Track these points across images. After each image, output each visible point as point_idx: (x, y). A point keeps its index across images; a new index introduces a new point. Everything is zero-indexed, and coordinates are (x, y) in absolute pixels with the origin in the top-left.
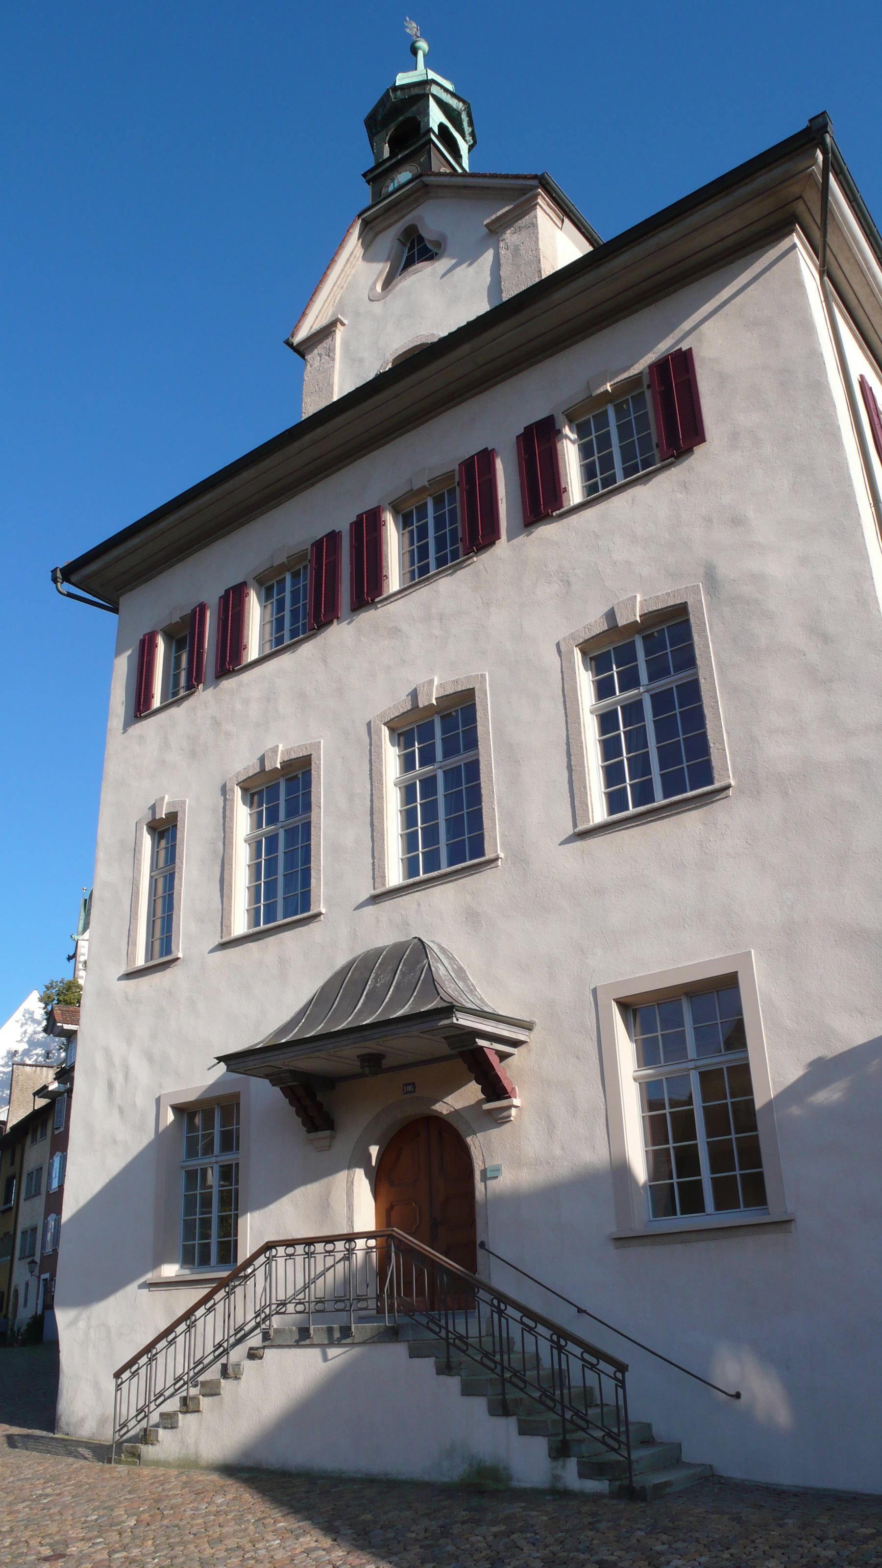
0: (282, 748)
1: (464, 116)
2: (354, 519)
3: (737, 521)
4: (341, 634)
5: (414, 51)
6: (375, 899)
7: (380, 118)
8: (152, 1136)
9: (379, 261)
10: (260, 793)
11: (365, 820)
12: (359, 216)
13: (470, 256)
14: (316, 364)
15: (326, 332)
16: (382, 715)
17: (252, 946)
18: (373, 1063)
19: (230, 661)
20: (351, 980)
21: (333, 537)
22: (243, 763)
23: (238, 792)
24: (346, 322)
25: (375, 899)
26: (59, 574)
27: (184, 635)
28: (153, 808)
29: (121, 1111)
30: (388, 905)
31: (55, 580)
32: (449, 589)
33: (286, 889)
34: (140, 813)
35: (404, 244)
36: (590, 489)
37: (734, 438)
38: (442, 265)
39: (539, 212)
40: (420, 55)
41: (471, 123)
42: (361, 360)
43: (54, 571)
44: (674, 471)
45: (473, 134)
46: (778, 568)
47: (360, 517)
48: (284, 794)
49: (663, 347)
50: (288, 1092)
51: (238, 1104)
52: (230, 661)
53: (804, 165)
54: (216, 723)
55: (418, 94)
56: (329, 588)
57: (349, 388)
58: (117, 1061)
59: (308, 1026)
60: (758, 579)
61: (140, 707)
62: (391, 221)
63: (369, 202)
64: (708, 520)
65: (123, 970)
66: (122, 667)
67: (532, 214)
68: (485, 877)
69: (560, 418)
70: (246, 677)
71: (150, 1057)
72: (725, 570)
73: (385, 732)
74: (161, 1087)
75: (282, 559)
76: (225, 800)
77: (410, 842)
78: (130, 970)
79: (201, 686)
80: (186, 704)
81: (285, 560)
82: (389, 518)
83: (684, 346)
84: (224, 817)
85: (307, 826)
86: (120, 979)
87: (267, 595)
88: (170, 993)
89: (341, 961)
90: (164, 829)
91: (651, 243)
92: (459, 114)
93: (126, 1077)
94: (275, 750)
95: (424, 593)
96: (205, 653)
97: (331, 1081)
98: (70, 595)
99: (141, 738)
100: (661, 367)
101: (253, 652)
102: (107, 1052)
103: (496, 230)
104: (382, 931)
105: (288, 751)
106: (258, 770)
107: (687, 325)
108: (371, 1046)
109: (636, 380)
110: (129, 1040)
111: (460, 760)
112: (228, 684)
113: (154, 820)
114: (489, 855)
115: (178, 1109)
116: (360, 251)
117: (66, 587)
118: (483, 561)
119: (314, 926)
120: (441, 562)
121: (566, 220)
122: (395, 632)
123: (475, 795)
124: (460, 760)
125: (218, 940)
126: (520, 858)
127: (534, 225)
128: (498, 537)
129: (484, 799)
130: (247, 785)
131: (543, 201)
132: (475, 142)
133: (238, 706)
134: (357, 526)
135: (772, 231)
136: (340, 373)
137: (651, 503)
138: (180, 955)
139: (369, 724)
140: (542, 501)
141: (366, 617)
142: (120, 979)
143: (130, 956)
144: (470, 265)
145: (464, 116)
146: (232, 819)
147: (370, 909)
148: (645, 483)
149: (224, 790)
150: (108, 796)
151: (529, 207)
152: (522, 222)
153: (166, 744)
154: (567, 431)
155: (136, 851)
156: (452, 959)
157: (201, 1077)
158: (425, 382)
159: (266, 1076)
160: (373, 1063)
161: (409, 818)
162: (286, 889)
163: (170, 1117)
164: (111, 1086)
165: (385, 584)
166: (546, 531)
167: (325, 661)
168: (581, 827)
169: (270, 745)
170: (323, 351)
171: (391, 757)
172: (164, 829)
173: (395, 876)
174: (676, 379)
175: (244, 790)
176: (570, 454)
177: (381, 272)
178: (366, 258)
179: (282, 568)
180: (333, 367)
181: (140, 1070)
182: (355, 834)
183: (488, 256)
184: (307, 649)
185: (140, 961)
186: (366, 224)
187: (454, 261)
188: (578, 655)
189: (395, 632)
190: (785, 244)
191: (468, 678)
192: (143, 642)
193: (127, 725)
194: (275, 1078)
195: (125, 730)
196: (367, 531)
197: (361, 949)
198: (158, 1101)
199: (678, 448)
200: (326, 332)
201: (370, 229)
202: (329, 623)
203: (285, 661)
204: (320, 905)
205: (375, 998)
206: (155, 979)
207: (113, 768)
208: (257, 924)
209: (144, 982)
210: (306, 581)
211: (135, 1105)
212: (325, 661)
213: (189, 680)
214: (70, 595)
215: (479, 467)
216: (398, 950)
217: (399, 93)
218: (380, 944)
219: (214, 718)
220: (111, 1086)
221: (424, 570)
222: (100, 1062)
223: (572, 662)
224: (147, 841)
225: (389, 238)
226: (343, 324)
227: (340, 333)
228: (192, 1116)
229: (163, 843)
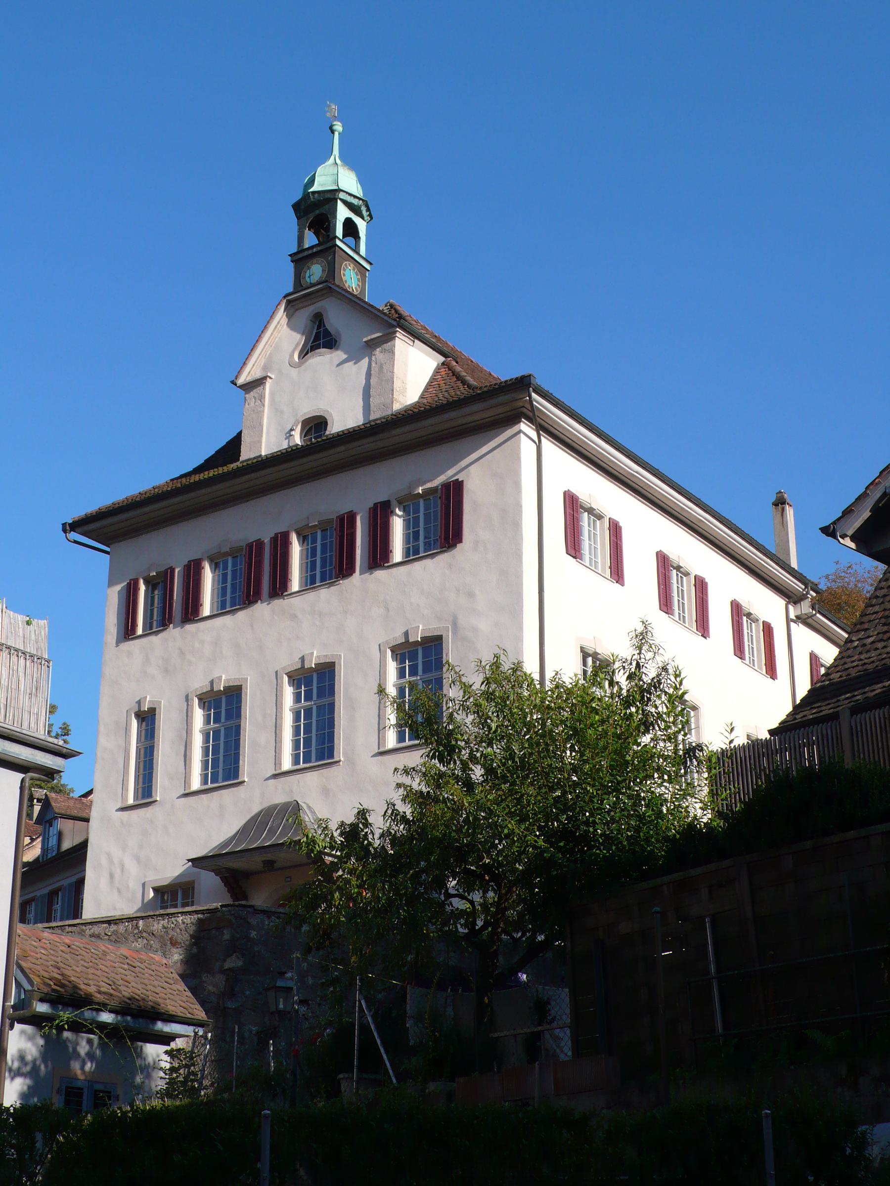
0: (225, 678)
1: (364, 209)
2: (273, 535)
3: (471, 595)
4: (262, 610)
5: (333, 132)
6: (275, 776)
7: (303, 207)
8: (140, 905)
9: (298, 332)
10: (210, 702)
11: (272, 728)
12: (285, 297)
13: (354, 357)
14: (252, 404)
15: (259, 382)
16: (284, 668)
17: (203, 796)
18: (269, 865)
19: (191, 612)
20: (258, 822)
21: (260, 544)
22: (200, 683)
23: (196, 701)
24: (273, 376)
25: (275, 776)
26: (68, 528)
27: (160, 582)
28: (139, 703)
29: (119, 891)
30: (282, 780)
31: (65, 531)
32: (326, 597)
33: (224, 765)
34: (128, 703)
35: (314, 322)
36: (407, 552)
37: (476, 543)
38: (339, 355)
39: (397, 341)
40: (336, 134)
41: (368, 210)
42: (282, 412)
43: (64, 525)
44: (446, 555)
45: (370, 215)
46: (484, 625)
47: (276, 534)
48: (224, 705)
49: (448, 475)
50: (225, 880)
51: (193, 888)
52: (191, 612)
53: (522, 396)
54: (182, 653)
55: (330, 198)
56: (255, 579)
57: (275, 449)
58: (116, 861)
59: (236, 845)
60: (475, 630)
61: (127, 632)
62: (306, 304)
63: (291, 290)
64: (458, 590)
65: (119, 806)
66: (114, 595)
67: (392, 342)
68: (334, 770)
69: (394, 503)
70: (201, 625)
71: (138, 859)
72: (461, 621)
73: (286, 678)
74: (145, 876)
75: (226, 549)
76: (188, 705)
77: (296, 745)
78: (124, 806)
79: (171, 626)
80: (161, 635)
81: (228, 550)
82: (294, 538)
83: (460, 477)
84: (187, 716)
85: (238, 727)
86: (117, 810)
87: (215, 566)
88: (151, 821)
89: (255, 810)
90: (147, 718)
91: (446, 416)
92: (359, 207)
93: (122, 871)
94: (220, 678)
95: (311, 596)
96: (174, 605)
97: (247, 875)
98: (76, 542)
99: (130, 654)
100: (446, 486)
101: (206, 611)
102: (109, 856)
103: (372, 345)
104: (278, 794)
105: (227, 680)
106: (209, 689)
107: (463, 463)
108: (268, 857)
109: (433, 491)
110: (124, 849)
111: (325, 701)
112: (189, 627)
113: (140, 710)
114: (336, 759)
115: (156, 890)
116: (285, 320)
117: (74, 536)
118: (345, 583)
119: (240, 788)
120: (323, 579)
121: (416, 341)
122: (294, 617)
123: (331, 724)
124: (325, 701)
125: (182, 792)
126: (351, 761)
127: (392, 352)
128: (354, 572)
129: (336, 726)
130: (202, 697)
131: (400, 334)
132: (371, 218)
133: (197, 645)
134: (274, 540)
135: (512, 419)
136: (268, 418)
137: (432, 570)
138: (158, 799)
139: (277, 672)
140: (379, 557)
141: (277, 602)
142: (117, 810)
143: (124, 797)
144: (355, 363)
145: (364, 209)
146: (192, 717)
147: (272, 781)
148: (432, 558)
149: (187, 699)
150: (105, 690)
151: (389, 337)
152: (387, 346)
153: (147, 661)
154: (397, 511)
155: (127, 730)
156: (313, 813)
157: (172, 869)
158: (322, 452)
159: (213, 871)
160: (269, 865)
161: (296, 731)
162: (224, 765)
163: (152, 894)
164: (112, 876)
165: (289, 584)
166: (379, 574)
167: (252, 626)
168: (382, 750)
169: (216, 675)
170: (256, 396)
171: (288, 692)
172: (147, 718)
173: (287, 764)
174: (454, 492)
175: (200, 699)
176: (398, 526)
177: (298, 344)
178: (289, 325)
179: (226, 554)
180: (263, 411)
181: (132, 867)
182: (266, 738)
183: (365, 362)
184: (242, 615)
185: (131, 801)
186: (289, 302)
187: (345, 356)
188: (389, 653)
189: (294, 617)
190: (515, 429)
191: (332, 655)
192: (129, 584)
193: (118, 643)
194: (217, 872)
195: (117, 644)
196: (281, 544)
197: (266, 805)
198: (144, 885)
199: (448, 543)
200: (259, 382)
201: (293, 305)
202: (256, 602)
203: (226, 620)
204: (245, 776)
205: (272, 832)
206: (141, 812)
207: (109, 671)
208: (206, 783)
209: (134, 814)
210: (242, 566)
211: (128, 887)
212: (252, 626)
213: (162, 620)
214: (76, 542)
215: (347, 522)
216: (286, 805)
217: (316, 195)
218: (277, 802)
219: (180, 650)
220: (112, 876)
221: (313, 582)
222: (104, 862)
223: (385, 657)
224: (134, 723)
225: (305, 315)
226: (270, 378)
227: (268, 384)
228: (163, 894)
229: (144, 724)
